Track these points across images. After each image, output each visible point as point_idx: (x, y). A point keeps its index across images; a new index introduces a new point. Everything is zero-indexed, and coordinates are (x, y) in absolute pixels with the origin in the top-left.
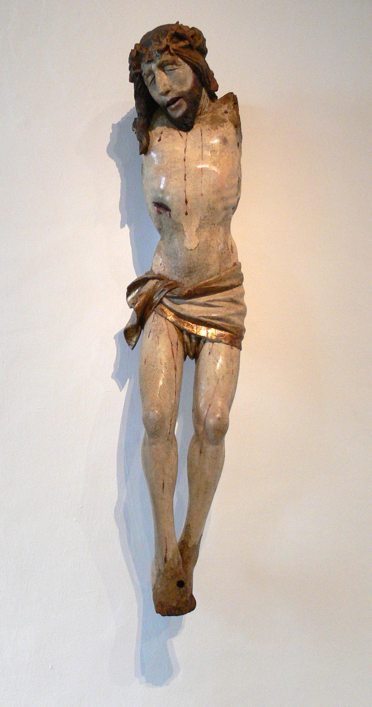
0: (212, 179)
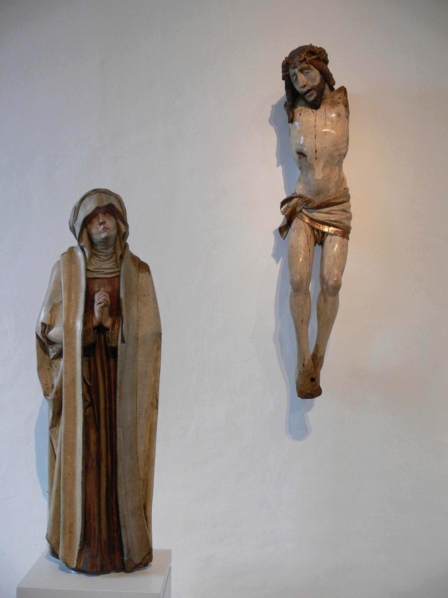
0: (331, 138)
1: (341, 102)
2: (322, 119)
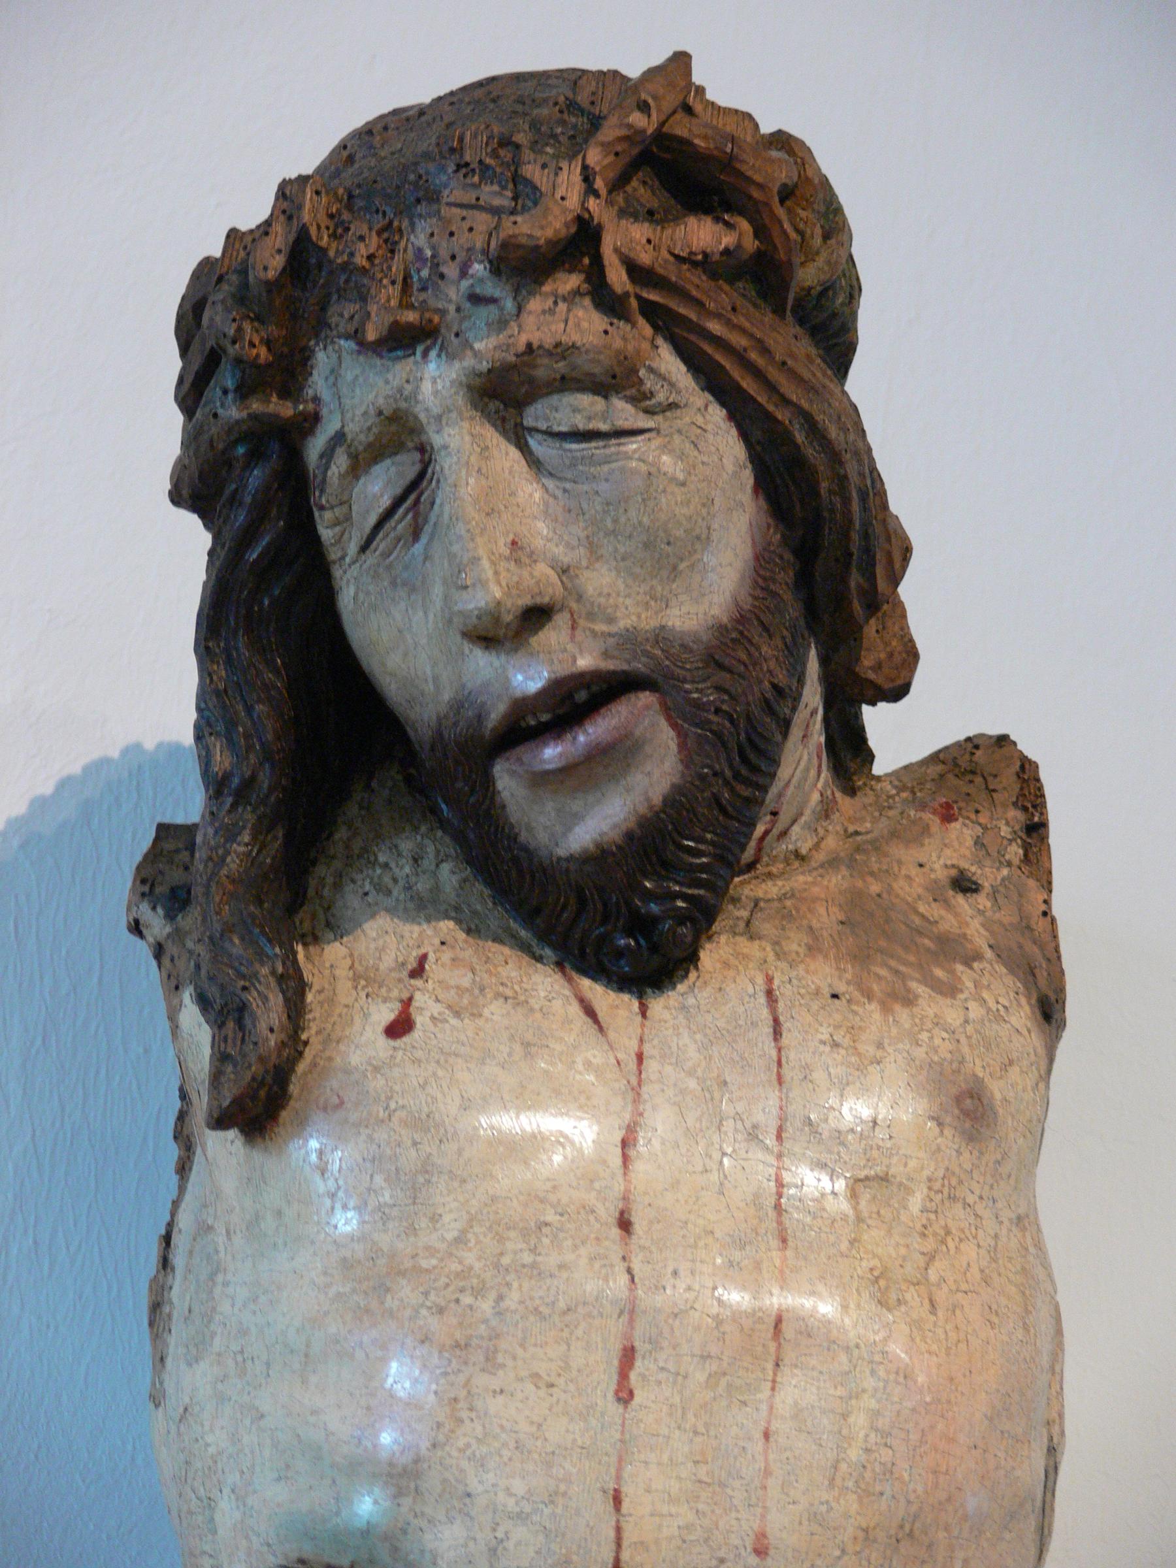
0: (859, 1420)
1: (979, 937)
2: (729, 1125)
